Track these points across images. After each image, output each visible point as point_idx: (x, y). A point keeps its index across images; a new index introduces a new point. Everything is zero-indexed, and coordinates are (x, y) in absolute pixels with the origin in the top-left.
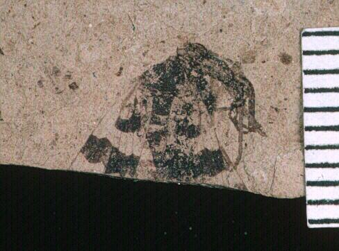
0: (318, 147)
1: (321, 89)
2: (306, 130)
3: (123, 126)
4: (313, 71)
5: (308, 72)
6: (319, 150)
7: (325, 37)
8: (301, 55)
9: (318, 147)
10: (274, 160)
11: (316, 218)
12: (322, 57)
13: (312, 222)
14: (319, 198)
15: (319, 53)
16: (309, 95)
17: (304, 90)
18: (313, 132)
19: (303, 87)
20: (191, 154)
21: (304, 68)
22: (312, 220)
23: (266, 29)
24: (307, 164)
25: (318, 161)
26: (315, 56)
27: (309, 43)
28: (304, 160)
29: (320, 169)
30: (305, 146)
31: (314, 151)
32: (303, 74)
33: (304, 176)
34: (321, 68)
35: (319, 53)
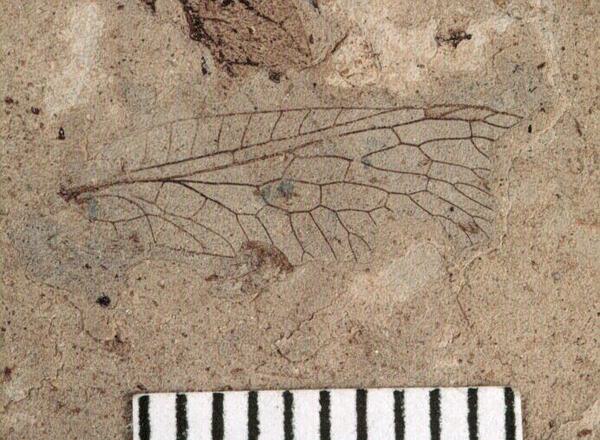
2: (321, 393)
5: (399, 397)
6: (282, 418)
7: (504, 431)
8: (394, 387)
10: (526, 317)
12: (465, 426)
13: (144, 403)
14: (190, 416)
15: (473, 419)
16: (391, 400)
17: (400, 390)
18: (318, 407)
19: (406, 390)
20: (109, 75)
21: (190, 397)
22: (147, 403)
24: (256, 395)
25: (262, 417)
26: (465, 411)
27: (491, 401)
28: (264, 388)
29: (246, 420)
32: (433, 389)
33: (487, 383)
34: (444, 424)
35: (473, 419)
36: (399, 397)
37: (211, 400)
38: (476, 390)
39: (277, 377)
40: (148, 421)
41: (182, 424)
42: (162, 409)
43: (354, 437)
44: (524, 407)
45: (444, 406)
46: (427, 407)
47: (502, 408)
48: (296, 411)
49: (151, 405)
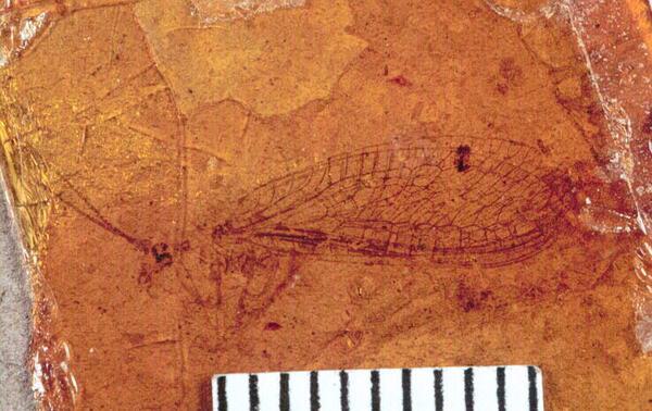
0: (344, 391)
1: (347, 390)
3: (194, 142)
4: (471, 384)
9: (344, 391)
11: (228, 388)
12: (495, 399)
13: (222, 382)
15: (501, 394)
16: (432, 378)
17: (437, 368)
18: (370, 385)
23: (233, 363)
26: (495, 386)
27: (517, 376)
29: (309, 396)
30: (346, 371)
31: (339, 385)
32: (466, 368)
35: (501, 394)
38: (504, 369)
49: (319, 378)
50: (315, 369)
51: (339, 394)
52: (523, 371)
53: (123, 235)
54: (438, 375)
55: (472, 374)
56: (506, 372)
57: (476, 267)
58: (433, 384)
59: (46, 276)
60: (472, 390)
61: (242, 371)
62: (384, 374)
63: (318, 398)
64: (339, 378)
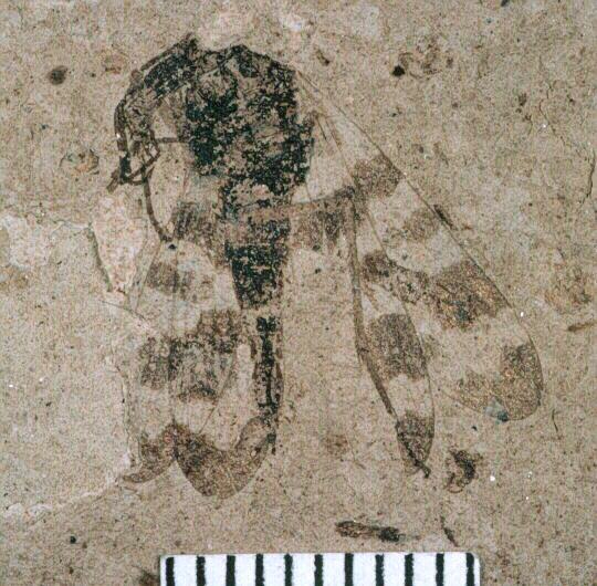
1: (172, 573)
11: (176, 570)
13: (170, 563)
14: (208, 575)
16: (373, 562)
17: (380, 554)
18: (313, 568)
21: (415, 556)
26: (434, 572)
27: (455, 563)
36: (201, 562)
37: (226, 561)
38: (443, 555)
39: (447, 432)
40: (173, 578)
41: (440, 579)
42: (185, 568)
43: (374, 583)
44: (482, 569)
45: (416, 568)
46: (403, 568)
47: (465, 569)
48: (296, 571)
49: (264, 560)
50: (261, 551)
51: (283, 576)
52: (461, 558)
53: (155, 224)
54: (380, 560)
55: (412, 559)
56: (446, 558)
57: (591, 266)
58: (374, 569)
59: (80, 506)
60: (412, 574)
61: (221, 553)
62: (297, 559)
63: (263, 580)
64: (283, 561)
